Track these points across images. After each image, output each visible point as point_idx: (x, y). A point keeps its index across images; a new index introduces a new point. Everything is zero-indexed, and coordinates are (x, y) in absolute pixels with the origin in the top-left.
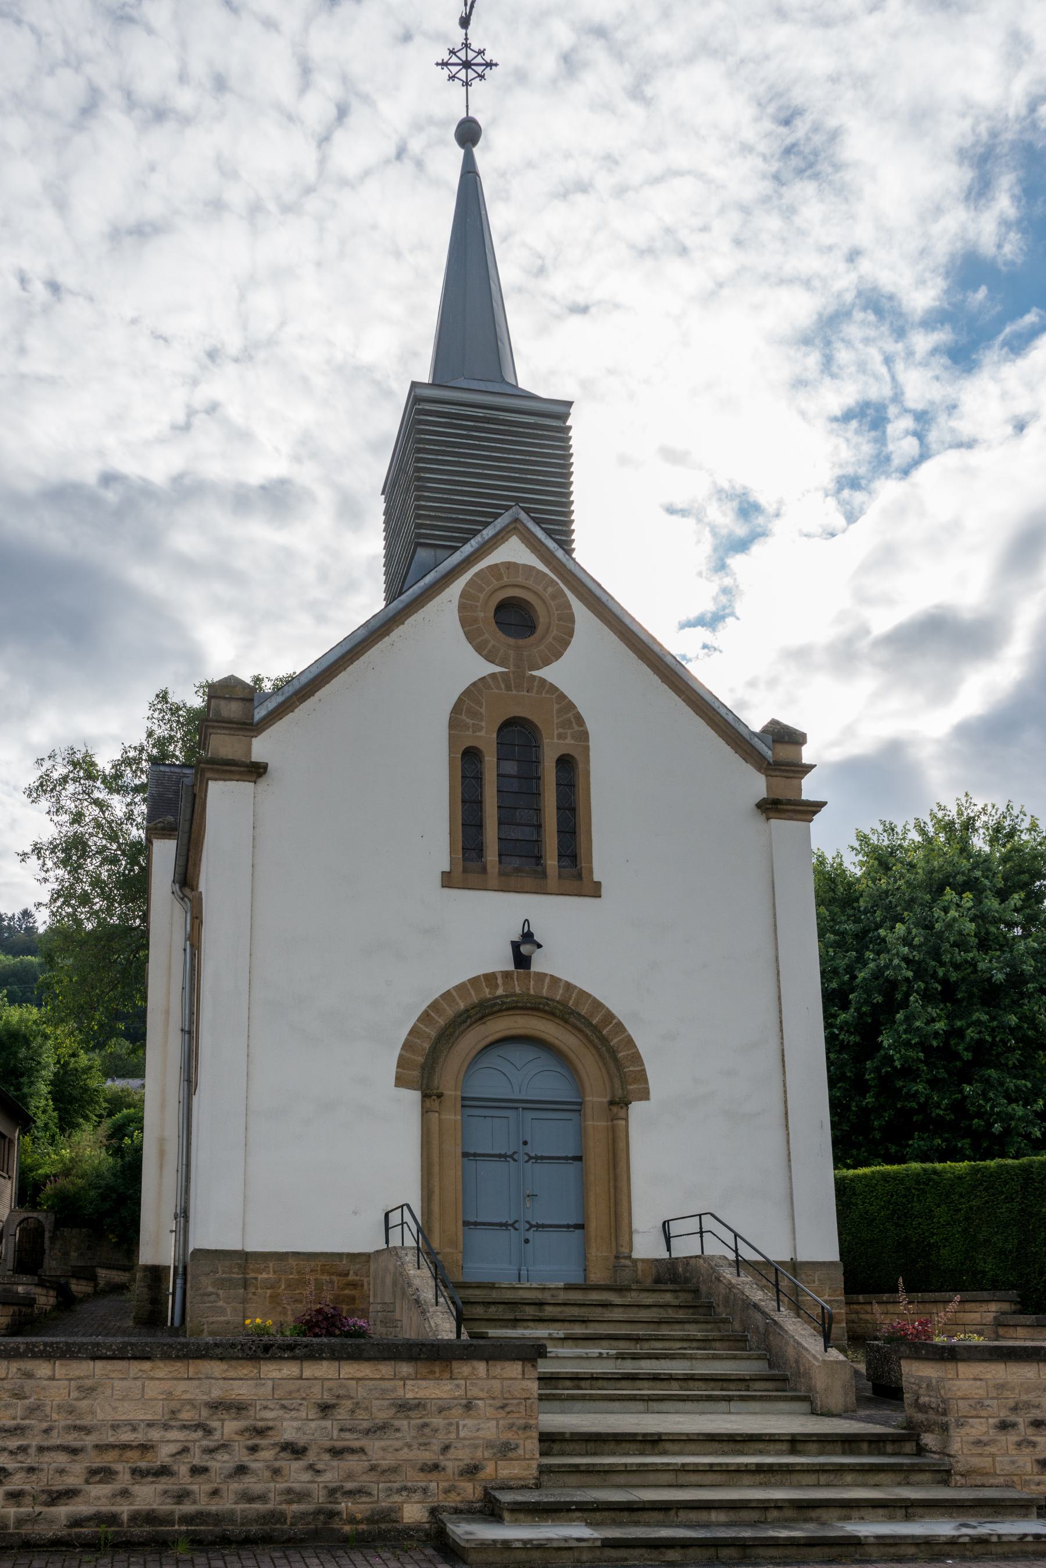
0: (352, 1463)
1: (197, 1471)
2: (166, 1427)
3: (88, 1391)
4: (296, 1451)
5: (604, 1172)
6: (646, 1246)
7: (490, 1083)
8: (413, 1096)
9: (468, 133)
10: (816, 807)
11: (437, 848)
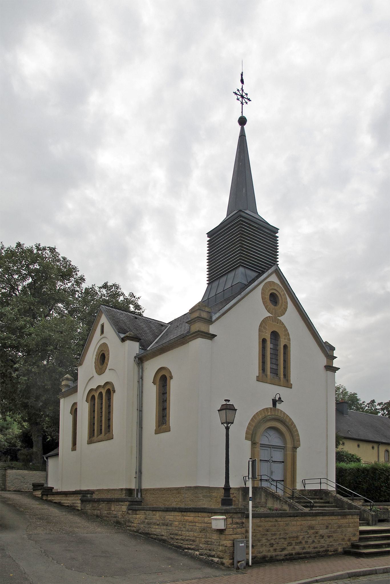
0: (331, 539)
1: (306, 542)
2: (301, 532)
3: (287, 525)
4: (322, 537)
5: (290, 466)
6: (299, 486)
7: (265, 441)
8: (249, 443)
9: (242, 121)
10: (214, 336)
11: (255, 370)
